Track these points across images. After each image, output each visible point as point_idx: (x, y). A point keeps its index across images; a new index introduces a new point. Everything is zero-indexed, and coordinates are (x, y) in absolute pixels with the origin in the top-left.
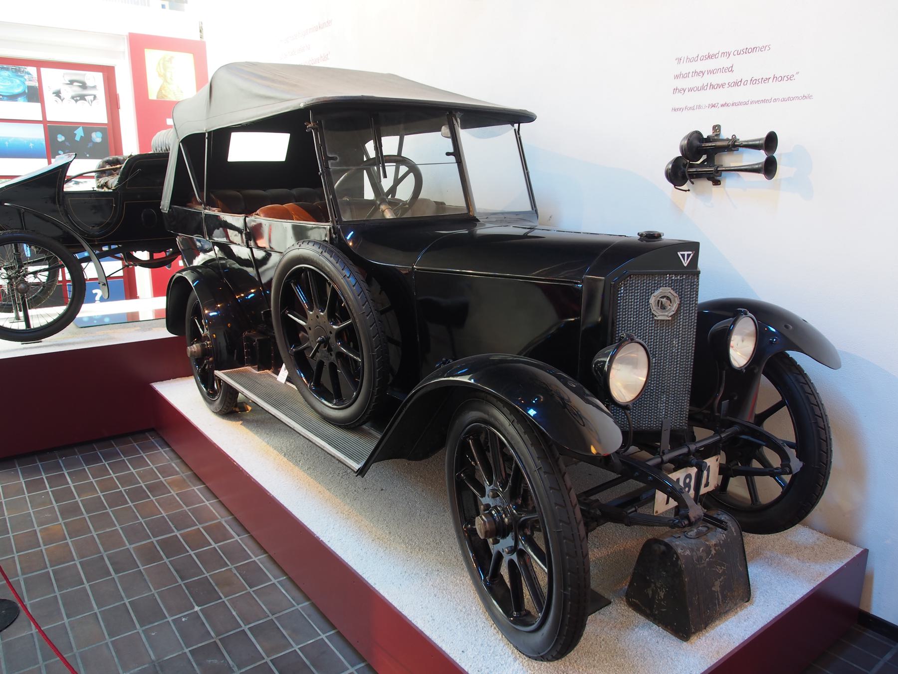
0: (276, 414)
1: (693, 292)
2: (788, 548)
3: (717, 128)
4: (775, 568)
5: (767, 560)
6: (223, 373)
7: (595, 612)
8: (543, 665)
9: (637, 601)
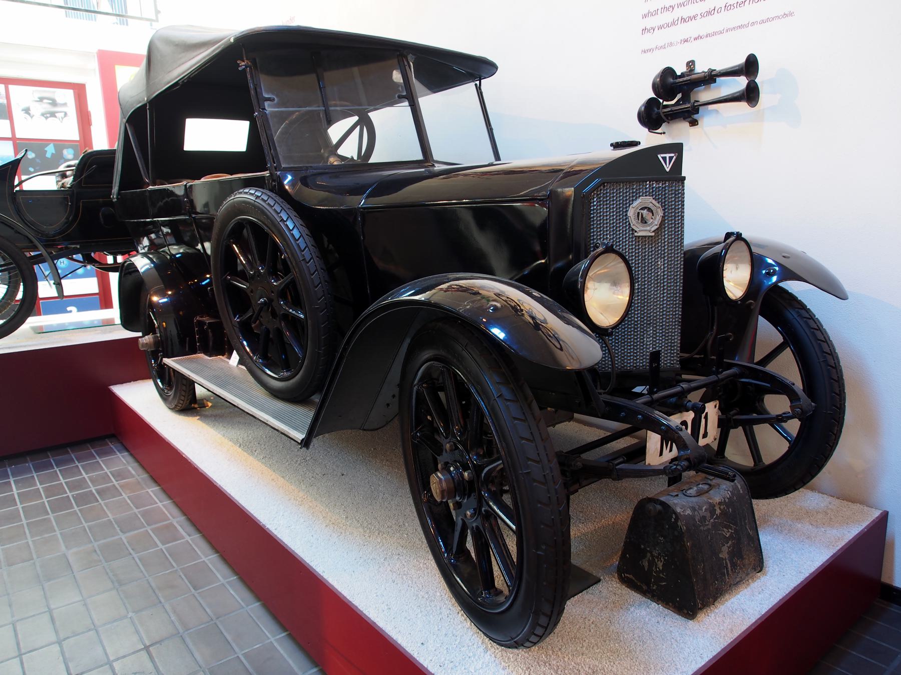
0: (220, 393)
1: (678, 201)
2: (798, 514)
3: (691, 64)
4: (787, 535)
5: (776, 527)
6: (172, 360)
7: (581, 592)
8: (520, 655)
9: (631, 576)
